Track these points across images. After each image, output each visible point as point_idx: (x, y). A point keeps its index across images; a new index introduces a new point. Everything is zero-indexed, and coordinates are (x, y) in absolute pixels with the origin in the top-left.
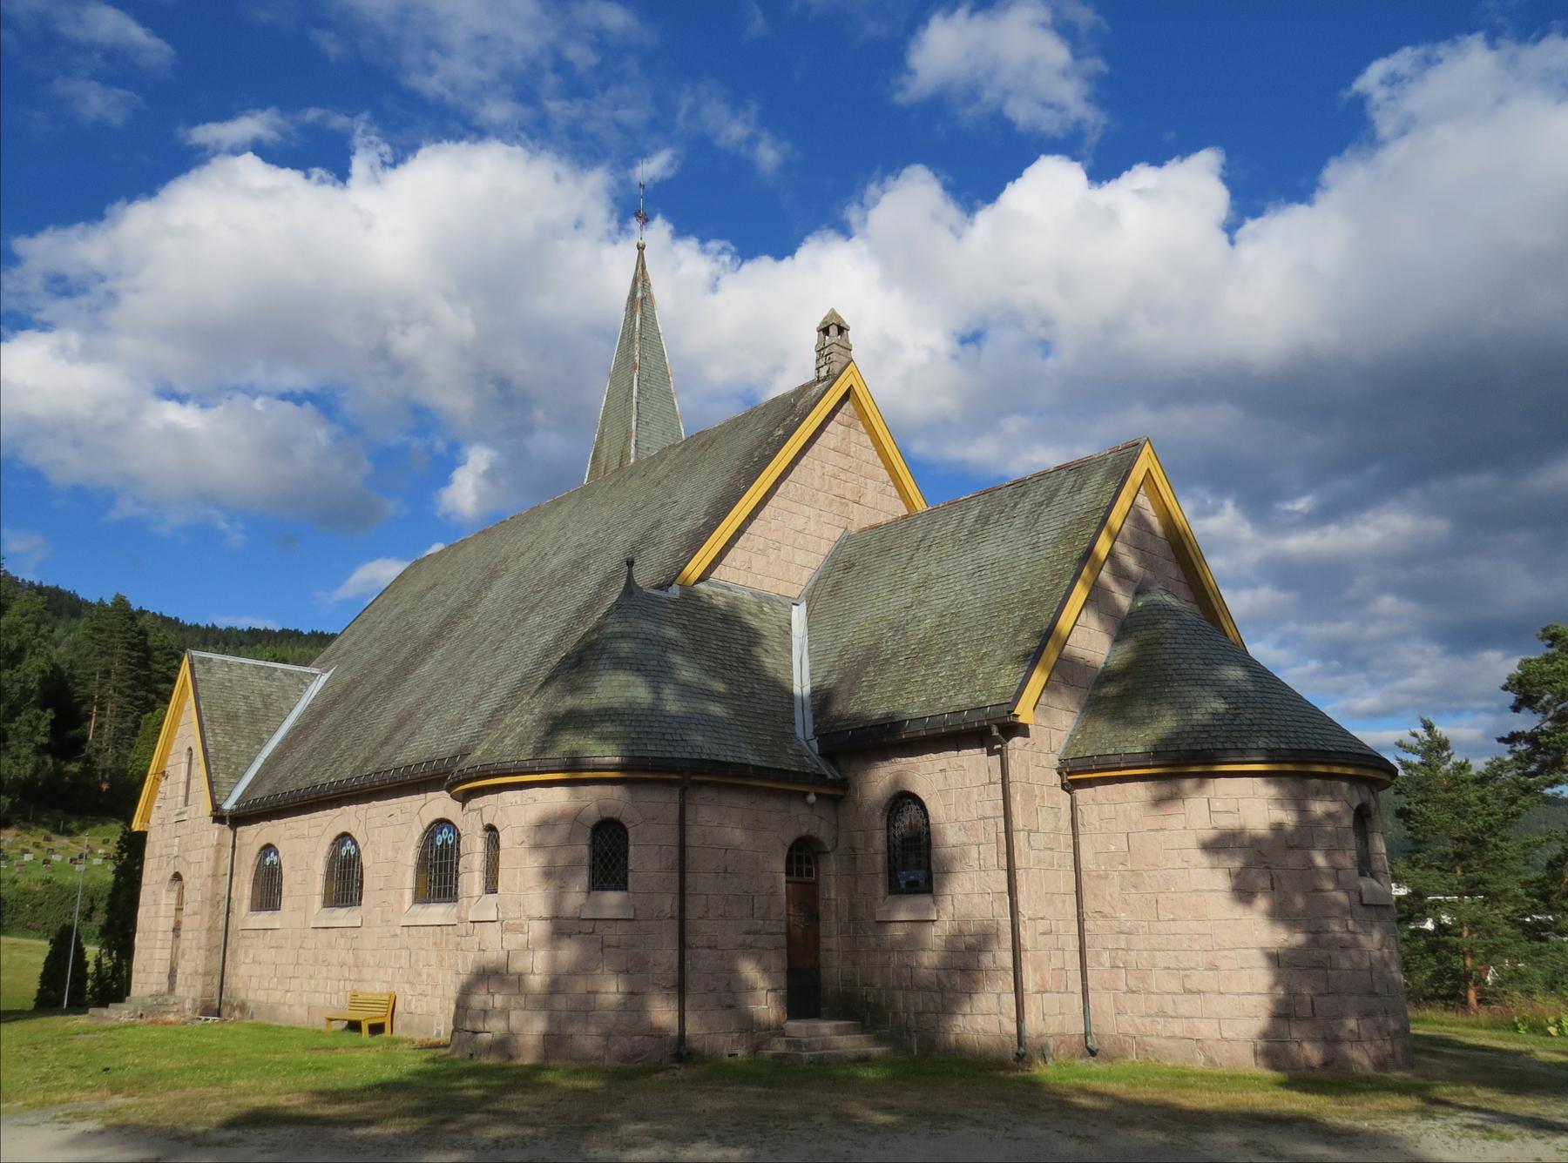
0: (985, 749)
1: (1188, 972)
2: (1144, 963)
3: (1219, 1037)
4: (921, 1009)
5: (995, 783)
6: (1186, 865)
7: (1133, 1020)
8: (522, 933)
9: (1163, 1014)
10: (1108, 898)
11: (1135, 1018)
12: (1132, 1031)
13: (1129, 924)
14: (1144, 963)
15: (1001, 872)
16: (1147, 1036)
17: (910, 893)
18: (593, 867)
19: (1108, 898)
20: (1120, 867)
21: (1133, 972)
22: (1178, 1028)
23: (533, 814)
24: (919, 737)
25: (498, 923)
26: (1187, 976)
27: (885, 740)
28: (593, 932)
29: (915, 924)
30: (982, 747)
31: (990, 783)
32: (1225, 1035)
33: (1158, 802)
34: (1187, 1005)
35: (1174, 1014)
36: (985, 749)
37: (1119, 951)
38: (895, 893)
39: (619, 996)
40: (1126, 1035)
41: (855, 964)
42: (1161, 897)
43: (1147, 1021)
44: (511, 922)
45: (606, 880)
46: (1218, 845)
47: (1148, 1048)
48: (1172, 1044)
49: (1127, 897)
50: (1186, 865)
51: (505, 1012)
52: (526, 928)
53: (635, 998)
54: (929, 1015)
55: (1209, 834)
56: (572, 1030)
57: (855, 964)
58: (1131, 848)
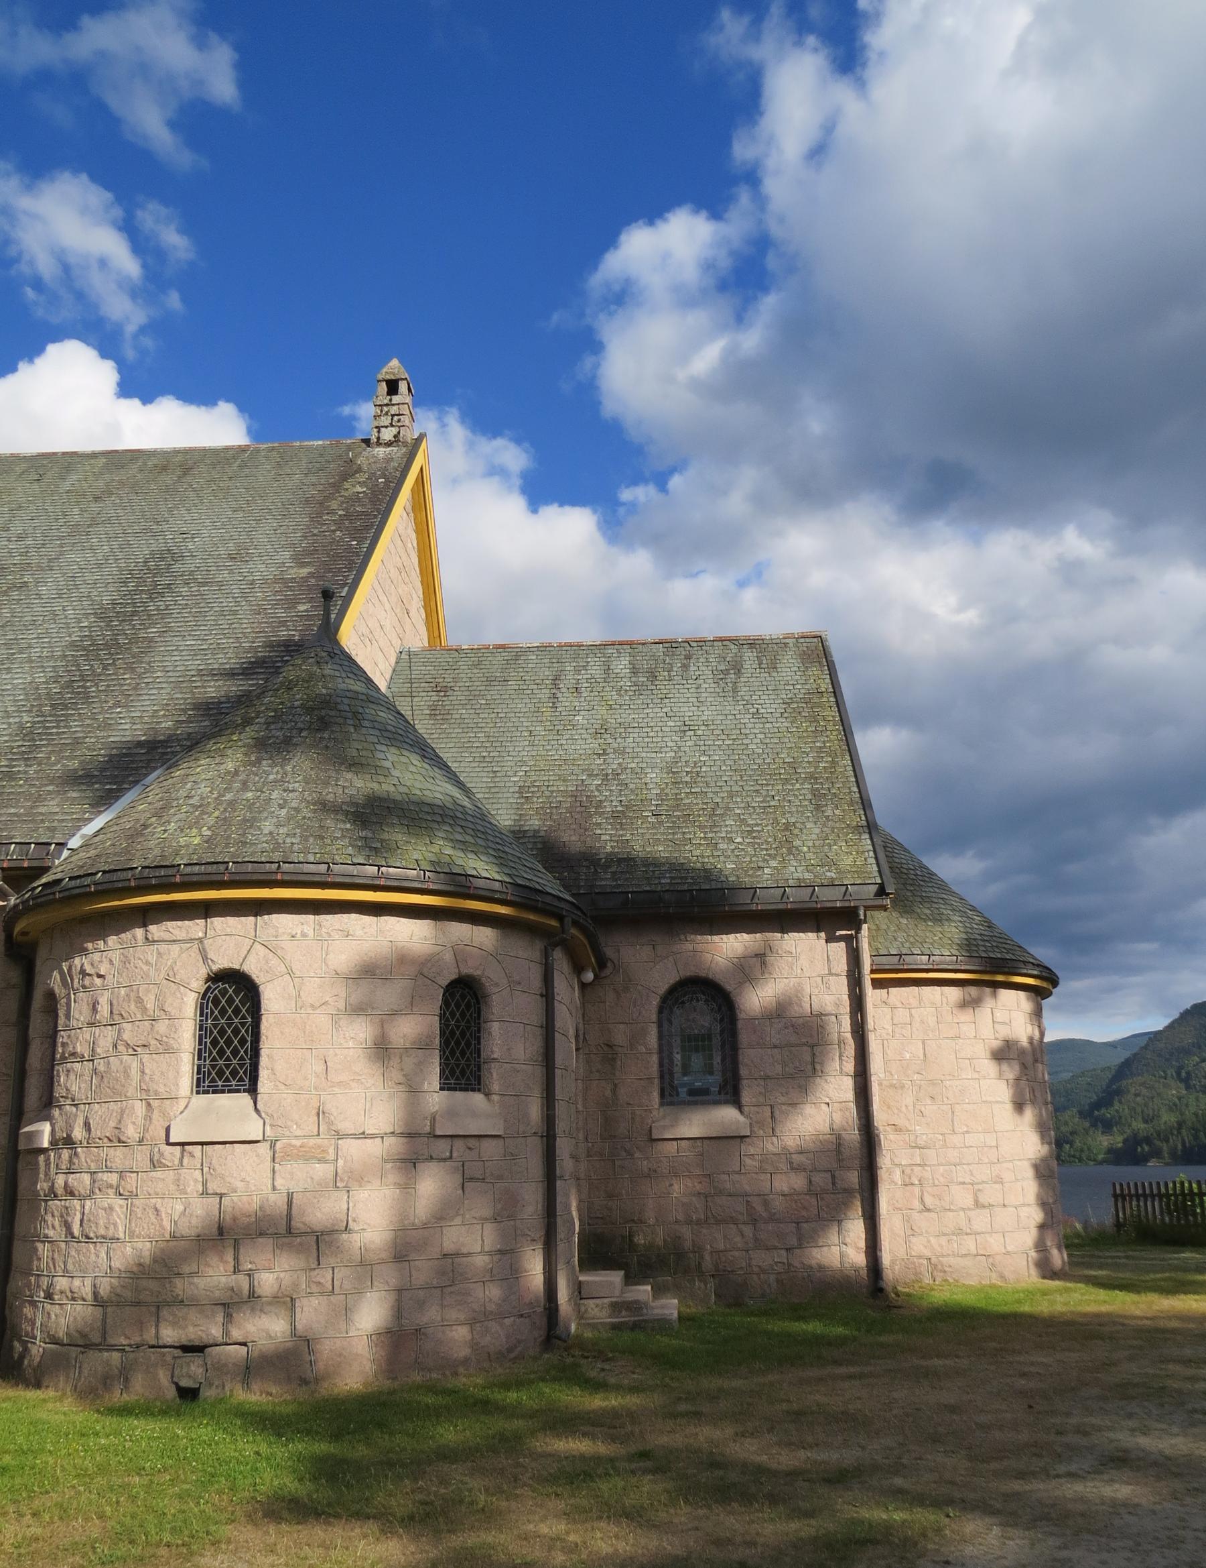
0: (823, 935)
1: (980, 1187)
2: (942, 1179)
3: (1004, 1251)
4: (722, 1247)
5: (837, 975)
6: (976, 1076)
7: (929, 1241)
8: (321, 1161)
9: (959, 1232)
10: (904, 1109)
11: (931, 1238)
12: (927, 1253)
13: (924, 1137)
14: (942, 1179)
15: (845, 1078)
16: (943, 1256)
17: (695, 1103)
18: (442, 1051)
19: (904, 1109)
20: (916, 1077)
21: (930, 1189)
22: (970, 1244)
23: (343, 957)
24: (750, 911)
25: (263, 1148)
26: (979, 1190)
27: (696, 910)
28: (451, 1157)
29: (713, 1141)
30: (818, 931)
31: (830, 974)
32: (1009, 1249)
33: (964, 1005)
34: (980, 1220)
35: (969, 1231)
36: (823, 935)
37: (914, 1167)
38: (671, 1104)
39: (486, 1258)
40: (920, 1257)
41: (610, 1196)
42: (957, 1108)
43: (943, 1240)
44: (298, 1143)
45: (220, 1074)
46: (1004, 1053)
47: (947, 1269)
48: (967, 1262)
49: (923, 1109)
50: (976, 1076)
51: (287, 1302)
52: (331, 1151)
53: (507, 1255)
54: (736, 1254)
55: (996, 1044)
56: (432, 1314)
57: (610, 1196)
58: (928, 1055)
